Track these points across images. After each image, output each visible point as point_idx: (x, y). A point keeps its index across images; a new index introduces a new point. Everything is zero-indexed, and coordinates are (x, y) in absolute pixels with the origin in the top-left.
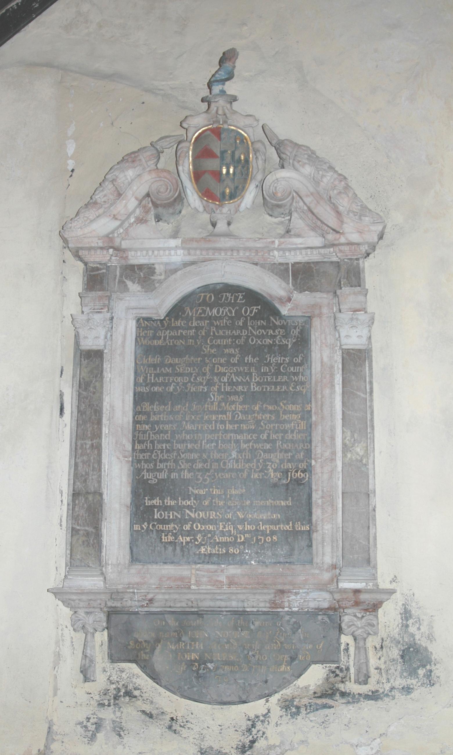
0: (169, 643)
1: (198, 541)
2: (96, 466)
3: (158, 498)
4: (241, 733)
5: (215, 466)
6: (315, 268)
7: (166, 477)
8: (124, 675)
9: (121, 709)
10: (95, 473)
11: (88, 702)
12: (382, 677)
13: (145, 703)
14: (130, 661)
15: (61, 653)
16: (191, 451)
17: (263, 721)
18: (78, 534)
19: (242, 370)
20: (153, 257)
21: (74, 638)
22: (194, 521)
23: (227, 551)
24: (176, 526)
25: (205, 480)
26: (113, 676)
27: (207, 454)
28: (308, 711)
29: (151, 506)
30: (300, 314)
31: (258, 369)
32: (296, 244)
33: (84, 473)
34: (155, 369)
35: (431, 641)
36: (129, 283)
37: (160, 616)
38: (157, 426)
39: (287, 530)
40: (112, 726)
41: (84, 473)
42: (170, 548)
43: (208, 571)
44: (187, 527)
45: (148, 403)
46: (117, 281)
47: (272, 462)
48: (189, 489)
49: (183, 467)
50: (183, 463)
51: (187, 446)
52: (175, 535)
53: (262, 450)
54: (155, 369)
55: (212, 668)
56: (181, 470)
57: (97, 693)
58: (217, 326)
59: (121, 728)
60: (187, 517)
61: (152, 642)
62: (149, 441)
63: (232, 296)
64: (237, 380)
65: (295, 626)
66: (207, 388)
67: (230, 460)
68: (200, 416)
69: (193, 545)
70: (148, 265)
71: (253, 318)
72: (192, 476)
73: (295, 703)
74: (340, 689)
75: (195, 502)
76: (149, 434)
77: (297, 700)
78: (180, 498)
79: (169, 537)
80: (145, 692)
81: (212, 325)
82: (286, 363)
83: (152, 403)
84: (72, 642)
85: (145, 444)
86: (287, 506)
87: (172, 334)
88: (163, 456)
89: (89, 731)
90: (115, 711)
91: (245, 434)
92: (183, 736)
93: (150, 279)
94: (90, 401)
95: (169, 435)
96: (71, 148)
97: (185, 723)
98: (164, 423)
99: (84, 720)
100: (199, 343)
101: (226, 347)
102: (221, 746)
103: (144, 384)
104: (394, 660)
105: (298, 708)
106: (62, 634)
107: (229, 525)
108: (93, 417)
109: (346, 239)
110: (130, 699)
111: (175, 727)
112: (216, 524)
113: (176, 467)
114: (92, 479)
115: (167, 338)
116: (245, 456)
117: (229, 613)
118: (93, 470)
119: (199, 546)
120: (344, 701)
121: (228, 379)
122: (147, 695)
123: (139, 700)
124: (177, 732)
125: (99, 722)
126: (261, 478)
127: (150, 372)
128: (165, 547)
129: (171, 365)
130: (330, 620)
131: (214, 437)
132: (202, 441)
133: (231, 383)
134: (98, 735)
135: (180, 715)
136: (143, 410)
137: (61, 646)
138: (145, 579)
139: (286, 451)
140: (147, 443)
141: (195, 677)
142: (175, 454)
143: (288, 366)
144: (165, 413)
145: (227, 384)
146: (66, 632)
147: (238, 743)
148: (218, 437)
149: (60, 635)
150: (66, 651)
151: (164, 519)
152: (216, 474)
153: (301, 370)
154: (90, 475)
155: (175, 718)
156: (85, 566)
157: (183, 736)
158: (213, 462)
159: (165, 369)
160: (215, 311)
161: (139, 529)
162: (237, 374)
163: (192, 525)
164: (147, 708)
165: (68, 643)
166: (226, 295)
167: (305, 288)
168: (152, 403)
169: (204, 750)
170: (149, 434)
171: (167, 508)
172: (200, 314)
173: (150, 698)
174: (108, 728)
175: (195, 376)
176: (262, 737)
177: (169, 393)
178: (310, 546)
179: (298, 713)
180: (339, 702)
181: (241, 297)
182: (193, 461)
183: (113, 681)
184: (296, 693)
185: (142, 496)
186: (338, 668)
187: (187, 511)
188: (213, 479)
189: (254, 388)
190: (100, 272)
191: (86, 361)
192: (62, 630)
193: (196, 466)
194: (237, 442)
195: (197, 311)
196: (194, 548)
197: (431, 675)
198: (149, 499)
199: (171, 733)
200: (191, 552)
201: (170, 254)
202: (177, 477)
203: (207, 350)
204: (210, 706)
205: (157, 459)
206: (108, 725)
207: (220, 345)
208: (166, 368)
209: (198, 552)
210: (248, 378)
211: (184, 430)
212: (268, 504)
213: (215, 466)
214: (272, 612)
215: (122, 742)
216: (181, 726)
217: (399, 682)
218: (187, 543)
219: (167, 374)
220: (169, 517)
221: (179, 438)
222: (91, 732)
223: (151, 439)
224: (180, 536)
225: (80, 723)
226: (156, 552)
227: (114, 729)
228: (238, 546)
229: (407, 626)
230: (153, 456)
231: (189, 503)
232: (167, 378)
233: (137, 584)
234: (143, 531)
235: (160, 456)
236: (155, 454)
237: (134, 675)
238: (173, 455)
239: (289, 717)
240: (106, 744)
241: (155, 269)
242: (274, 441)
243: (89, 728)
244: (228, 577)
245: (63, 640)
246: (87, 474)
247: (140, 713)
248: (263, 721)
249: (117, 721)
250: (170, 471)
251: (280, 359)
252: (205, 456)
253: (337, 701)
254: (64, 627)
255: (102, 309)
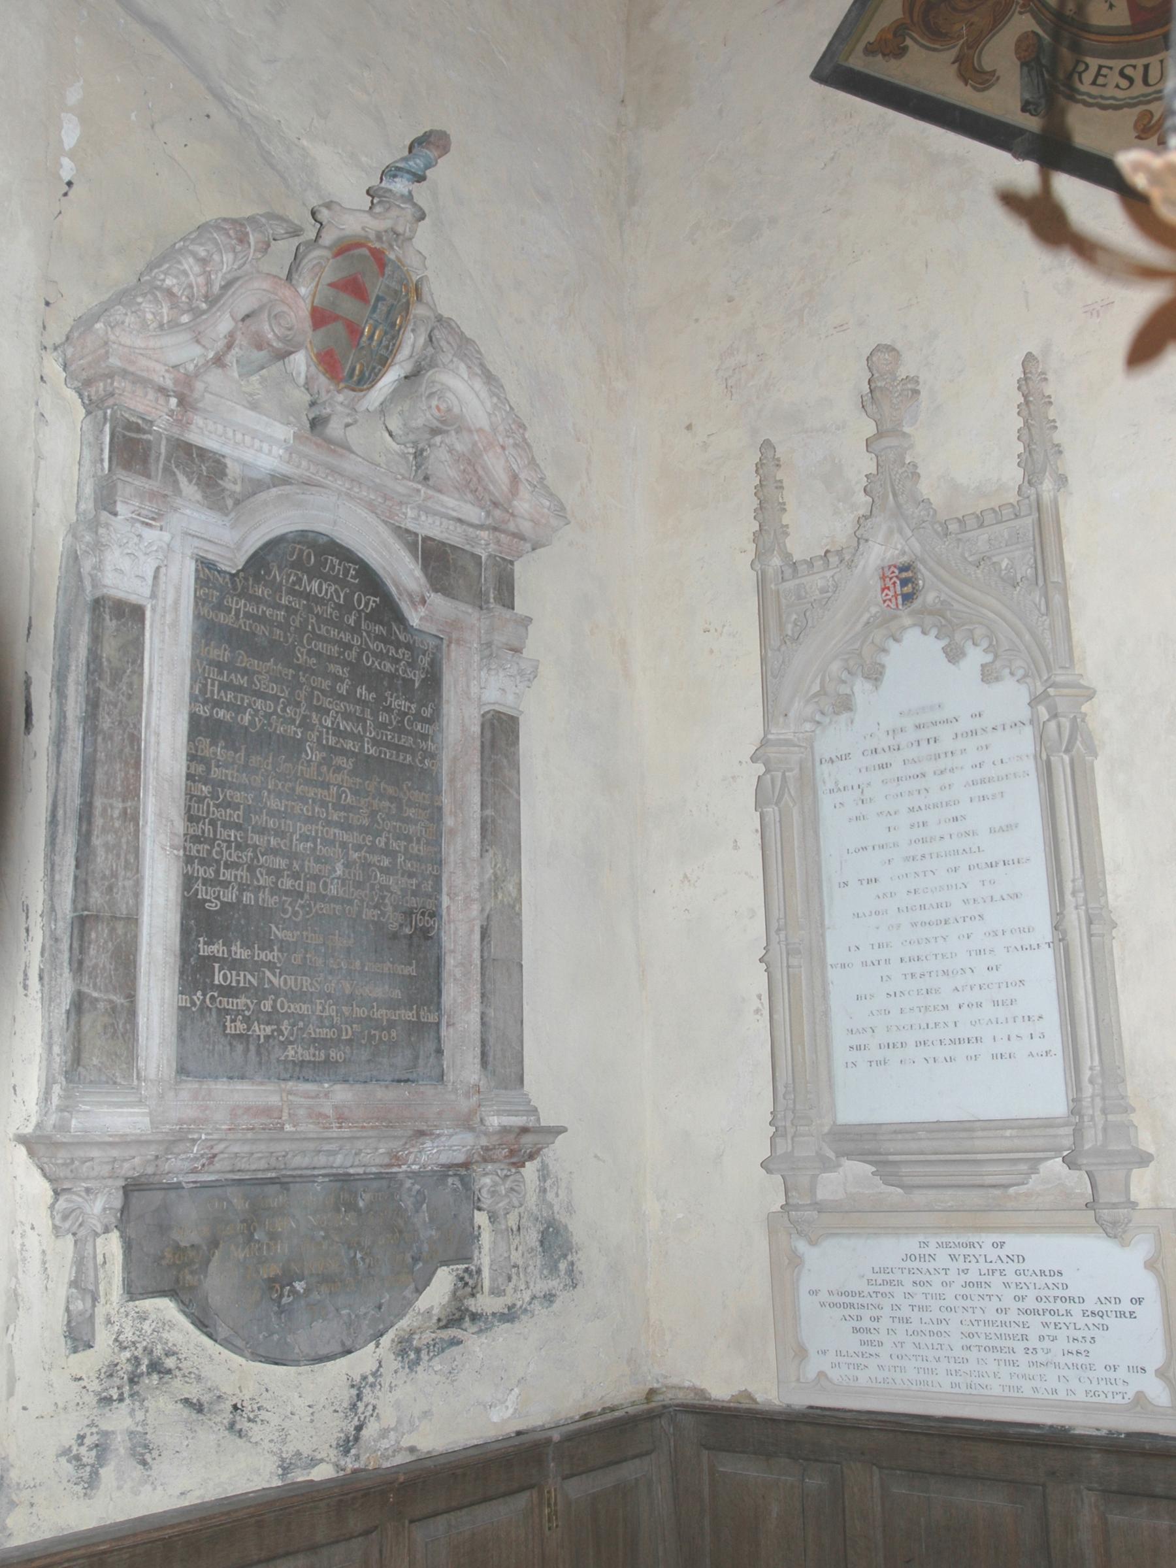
0: (233, 1247)
1: (283, 1036)
2: (132, 861)
3: (221, 941)
4: (342, 1414)
5: (311, 887)
6: (451, 557)
7: (234, 901)
8: (147, 1327)
9: (146, 1403)
10: (129, 874)
11: (78, 1400)
12: (520, 1279)
13: (187, 1383)
14: (162, 1293)
15: (19, 1291)
16: (275, 852)
17: (372, 1385)
18: (96, 1009)
19: (353, 710)
20: (232, 442)
21: (48, 1252)
22: (276, 992)
23: (328, 1056)
24: (249, 1001)
25: (295, 914)
26: (126, 1331)
27: (300, 862)
28: (432, 1354)
29: (209, 957)
30: (434, 632)
31: (375, 715)
32: (447, 508)
33: (107, 872)
34: (221, 673)
35: (571, 1214)
36: (182, 479)
37: (219, 1191)
38: (222, 791)
39: (410, 1021)
40: (129, 1445)
41: (107, 872)
42: (240, 1048)
43: (307, 1095)
44: (267, 1006)
45: (208, 741)
46: (161, 466)
47: (392, 893)
48: (270, 927)
49: (262, 882)
50: (262, 874)
51: (269, 841)
52: (247, 1020)
53: (378, 867)
54: (221, 673)
55: (302, 1291)
56: (259, 887)
57: (93, 1375)
58: (317, 615)
59: (146, 1446)
60: (266, 986)
61: (205, 1248)
62: (207, 820)
63: (340, 565)
64: (345, 728)
65: (418, 1198)
66: (302, 733)
67: (333, 879)
68: (291, 785)
69: (276, 1041)
70: (215, 453)
71: (369, 617)
72: (275, 903)
73: (415, 1343)
74: (470, 1309)
75: (280, 954)
76: (208, 805)
77: (416, 1337)
78: (256, 946)
79: (238, 1023)
80: (185, 1359)
81: (311, 611)
82: (412, 715)
83: (214, 743)
84: (44, 1263)
85: (200, 825)
86: (410, 976)
87: (250, 609)
88: (230, 855)
89: (85, 1466)
90: (133, 1410)
91: (355, 834)
92: (253, 1440)
93: (218, 485)
94: (120, 714)
95: (241, 813)
96: (70, 135)
97: (257, 1412)
98: (232, 786)
99: (73, 1442)
100: (290, 640)
101: (330, 659)
102: (315, 1447)
103: (201, 699)
104: (532, 1249)
105: (418, 1351)
106: (23, 1245)
107: (330, 1005)
108: (127, 750)
109: (517, 526)
110: (160, 1378)
111: (242, 1424)
112: (311, 1002)
113: (252, 881)
114: (124, 888)
115: (241, 616)
116: (355, 875)
117: (327, 1179)
118: (126, 868)
119: (284, 1045)
120: (475, 1329)
121: (333, 723)
122: (189, 1363)
123: (176, 1377)
124: (243, 1433)
125: (102, 1440)
126: (376, 919)
127: (211, 676)
128: (231, 1044)
129: (245, 672)
130: (462, 1185)
131: (311, 831)
132: (291, 836)
133: (337, 732)
134: (101, 1471)
135: (247, 1397)
136: (199, 753)
137: (20, 1275)
138: (207, 1112)
139: (411, 875)
140: (204, 824)
141: (275, 1313)
142: (249, 854)
143: (414, 720)
144: (236, 766)
145: (331, 732)
146: (32, 1239)
147: (339, 1435)
148: (317, 831)
149: (19, 1247)
150: (31, 1285)
151: (230, 986)
152: (312, 903)
153: (431, 732)
154: (121, 878)
155: (239, 1406)
156: (107, 1083)
157: (253, 1440)
158: (308, 879)
159: (236, 677)
160: (315, 585)
161: (188, 1005)
162: (347, 716)
163: (275, 1001)
164: (193, 1392)
165: (35, 1266)
166: (332, 561)
167: (438, 586)
168: (214, 743)
169: (288, 1461)
170: (208, 805)
171: (234, 964)
172: (294, 583)
173: (194, 1370)
174: (122, 1451)
175: (283, 703)
176: (372, 1415)
177: (242, 727)
178: (439, 1052)
179: (417, 1362)
180: (467, 1332)
181: (352, 572)
182: (278, 873)
183: (125, 1344)
184: (415, 1324)
185: (194, 934)
186: (466, 1270)
187: (268, 973)
188: (308, 913)
189: (369, 750)
190: (145, 437)
191: (114, 622)
192: (22, 1236)
193: (282, 884)
194: (344, 845)
195: (289, 576)
196: (277, 1048)
197: (573, 1271)
198: (205, 943)
199: (233, 1437)
200: (272, 1057)
201: (260, 450)
202: (253, 903)
203: (302, 658)
204: (292, 1369)
205: (221, 859)
206: (120, 1444)
207: (322, 653)
208: (239, 676)
209: (283, 1058)
210: (360, 728)
211: (264, 808)
212: (386, 970)
213: (311, 887)
214: (387, 1173)
215: (149, 1476)
216: (249, 1420)
217: (541, 1286)
218: (267, 1037)
219: (239, 689)
220: (238, 982)
221: (257, 823)
222: (88, 1469)
223: (211, 816)
224: (256, 1023)
225: (66, 1452)
226: (216, 1055)
227: (133, 1452)
228: (342, 1048)
229: (544, 1191)
230: (214, 851)
231: (270, 957)
232: (239, 695)
233: (194, 1122)
234: (194, 1009)
235: (226, 854)
236: (217, 848)
237: (164, 1324)
238: (246, 856)
239: (407, 1370)
240: (119, 1488)
241: (225, 466)
242: (392, 854)
243: (85, 1460)
244: (336, 1107)
245: (24, 1260)
246: (114, 875)
247: (180, 1406)
248: (372, 1385)
249: (138, 1432)
250: (242, 888)
251: (404, 704)
252: (296, 866)
253: (466, 1330)
254: (28, 1227)
255: (153, 519)
